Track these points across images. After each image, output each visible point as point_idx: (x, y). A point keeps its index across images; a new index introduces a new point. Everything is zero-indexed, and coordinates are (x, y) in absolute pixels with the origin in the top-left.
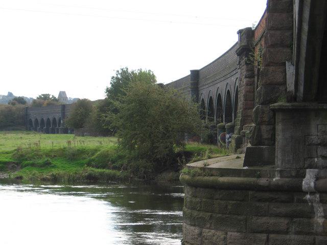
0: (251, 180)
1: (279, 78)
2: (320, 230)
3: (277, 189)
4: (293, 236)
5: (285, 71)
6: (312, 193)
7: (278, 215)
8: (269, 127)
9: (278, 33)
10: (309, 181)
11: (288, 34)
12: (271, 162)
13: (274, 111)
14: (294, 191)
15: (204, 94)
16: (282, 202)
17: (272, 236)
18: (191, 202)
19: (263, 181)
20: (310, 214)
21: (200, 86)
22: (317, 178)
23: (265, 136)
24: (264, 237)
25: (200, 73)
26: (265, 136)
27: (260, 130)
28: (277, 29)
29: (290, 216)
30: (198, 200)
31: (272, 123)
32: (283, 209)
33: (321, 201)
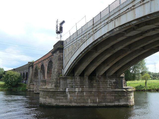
0: (57, 90)
1: (61, 72)
2: (69, 99)
3: (62, 92)
4: (64, 100)
5: (62, 71)
6: (68, 92)
7: (62, 96)
8: (59, 81)
9: (61, 64)
10: (67, 90)
11: (62, 64)
12: (59, 87)
13: (60, 78)
14: (64, 92)
15: (102, 16)
16: (62, 94)
17: (60, 100)
18: (43, 94)
19: (59, 90)
20: (67, 96)
21: (64, 46)
22: (69, 90)
23: (59, 82)
24: (59, 100)
25: (65, 43)
26: (59, 82)
27: (57, 81)
28: (61, 64)
29: (64, 96)
30: (45, 94)
31: (59, 80)
32: (62, 95)
33: (69, 94)
